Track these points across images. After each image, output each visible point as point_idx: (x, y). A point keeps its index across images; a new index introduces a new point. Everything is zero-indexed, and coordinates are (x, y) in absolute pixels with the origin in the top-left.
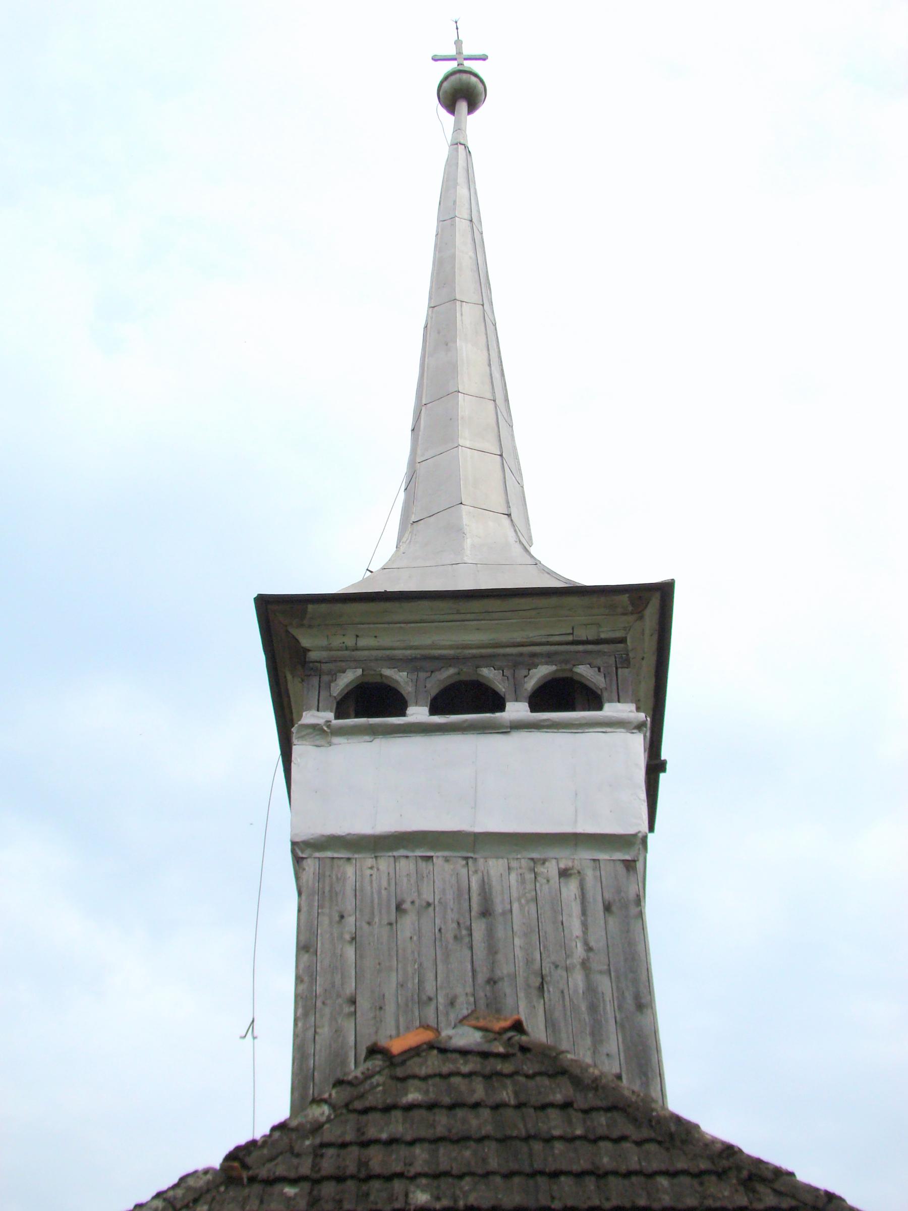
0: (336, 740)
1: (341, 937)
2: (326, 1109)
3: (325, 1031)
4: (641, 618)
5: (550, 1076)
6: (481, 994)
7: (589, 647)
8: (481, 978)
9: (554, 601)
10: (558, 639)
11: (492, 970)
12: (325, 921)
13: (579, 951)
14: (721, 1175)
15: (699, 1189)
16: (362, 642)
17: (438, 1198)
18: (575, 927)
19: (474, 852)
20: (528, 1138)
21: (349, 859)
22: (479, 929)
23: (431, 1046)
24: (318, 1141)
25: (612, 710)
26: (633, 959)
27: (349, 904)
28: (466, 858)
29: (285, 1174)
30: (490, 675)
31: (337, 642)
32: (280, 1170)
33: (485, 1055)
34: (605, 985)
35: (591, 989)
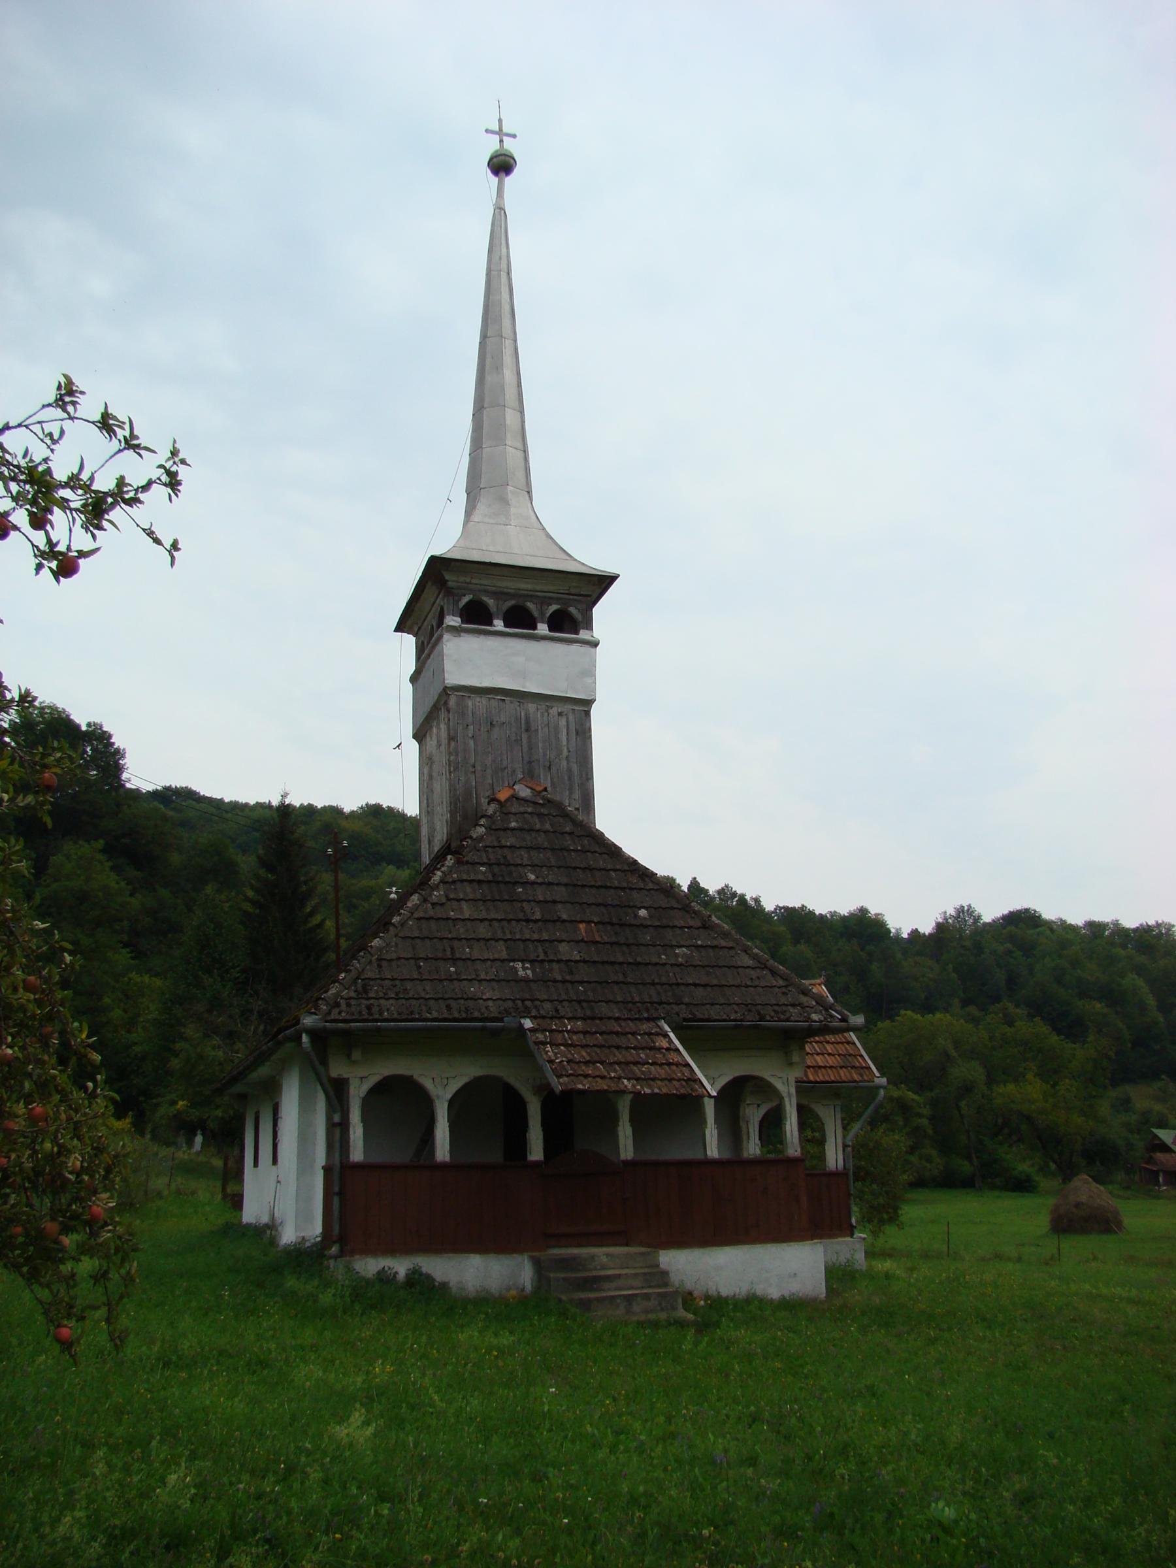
2: (483, 829)
7: (575, 597)
8: (526, 759)
13: (565, 752)
16: (473, 581)
18: (564, 738)
21: (469, 697)
22: (525, 737)
31: (462, 579)
34: (575, 767)
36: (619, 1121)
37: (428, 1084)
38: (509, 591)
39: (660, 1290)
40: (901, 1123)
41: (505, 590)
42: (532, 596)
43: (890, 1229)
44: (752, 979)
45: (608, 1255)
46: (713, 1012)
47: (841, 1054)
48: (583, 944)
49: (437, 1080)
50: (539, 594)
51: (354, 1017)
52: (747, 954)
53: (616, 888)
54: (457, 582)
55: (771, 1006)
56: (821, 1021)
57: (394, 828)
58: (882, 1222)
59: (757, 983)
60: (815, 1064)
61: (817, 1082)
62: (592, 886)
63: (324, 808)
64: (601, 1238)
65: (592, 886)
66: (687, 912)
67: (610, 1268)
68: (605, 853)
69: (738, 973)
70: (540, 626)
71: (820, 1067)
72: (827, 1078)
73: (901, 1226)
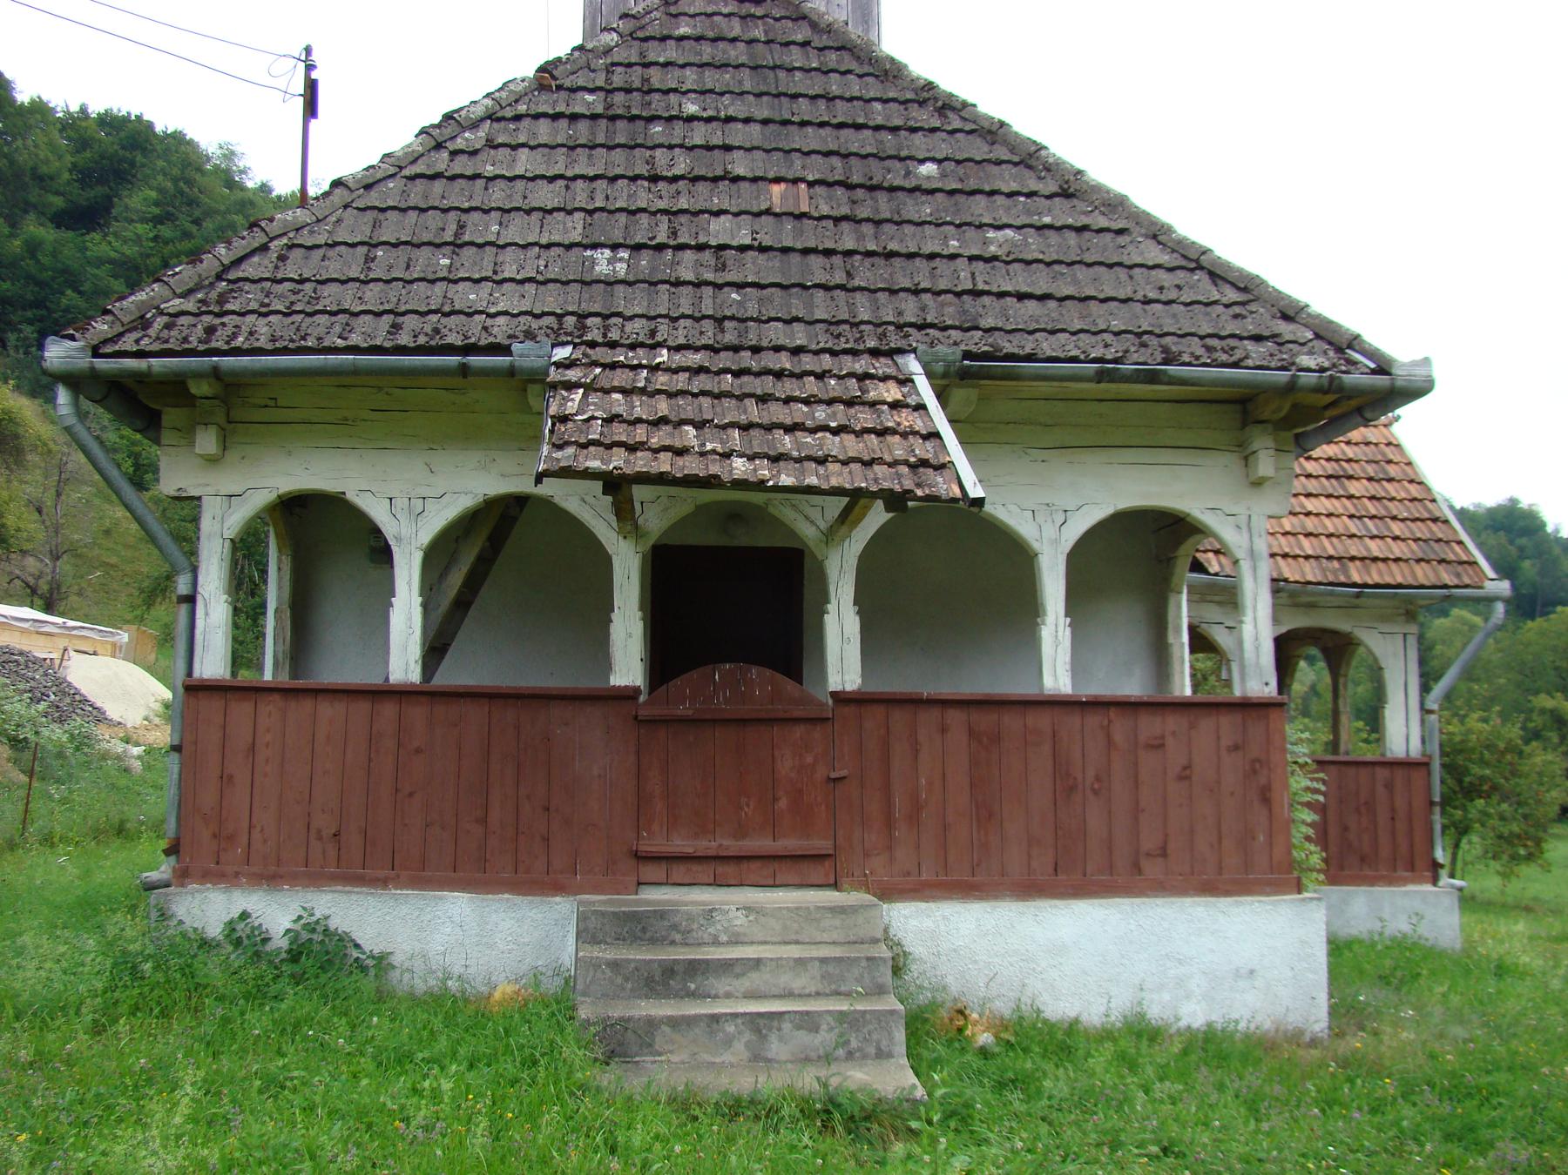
14: (922, 103)
32: (581, 83)
36: (828, 602)
37: (377, 511)
39: (844, 1007)
40: (1556, 740)
43: (1528, 870)
44: (1161, 288)
45: (748, 909)
46: (1048, 346)
47: (1419, 539)
48: (770, 219)
52: (1159, 243)
53: (877, 128)
55: (1202, 338)
56: (1322, 370)
58: (1514, 858)
59: (1173, 295)
60: (1365, 554)
61: (1366, 586)
62: (822, 125)
65: (822, 125)
66: (1030, 167)
69: (1131, 277)
71: (1375, 559)
72: (1389, 580)
73: (1547, 868)
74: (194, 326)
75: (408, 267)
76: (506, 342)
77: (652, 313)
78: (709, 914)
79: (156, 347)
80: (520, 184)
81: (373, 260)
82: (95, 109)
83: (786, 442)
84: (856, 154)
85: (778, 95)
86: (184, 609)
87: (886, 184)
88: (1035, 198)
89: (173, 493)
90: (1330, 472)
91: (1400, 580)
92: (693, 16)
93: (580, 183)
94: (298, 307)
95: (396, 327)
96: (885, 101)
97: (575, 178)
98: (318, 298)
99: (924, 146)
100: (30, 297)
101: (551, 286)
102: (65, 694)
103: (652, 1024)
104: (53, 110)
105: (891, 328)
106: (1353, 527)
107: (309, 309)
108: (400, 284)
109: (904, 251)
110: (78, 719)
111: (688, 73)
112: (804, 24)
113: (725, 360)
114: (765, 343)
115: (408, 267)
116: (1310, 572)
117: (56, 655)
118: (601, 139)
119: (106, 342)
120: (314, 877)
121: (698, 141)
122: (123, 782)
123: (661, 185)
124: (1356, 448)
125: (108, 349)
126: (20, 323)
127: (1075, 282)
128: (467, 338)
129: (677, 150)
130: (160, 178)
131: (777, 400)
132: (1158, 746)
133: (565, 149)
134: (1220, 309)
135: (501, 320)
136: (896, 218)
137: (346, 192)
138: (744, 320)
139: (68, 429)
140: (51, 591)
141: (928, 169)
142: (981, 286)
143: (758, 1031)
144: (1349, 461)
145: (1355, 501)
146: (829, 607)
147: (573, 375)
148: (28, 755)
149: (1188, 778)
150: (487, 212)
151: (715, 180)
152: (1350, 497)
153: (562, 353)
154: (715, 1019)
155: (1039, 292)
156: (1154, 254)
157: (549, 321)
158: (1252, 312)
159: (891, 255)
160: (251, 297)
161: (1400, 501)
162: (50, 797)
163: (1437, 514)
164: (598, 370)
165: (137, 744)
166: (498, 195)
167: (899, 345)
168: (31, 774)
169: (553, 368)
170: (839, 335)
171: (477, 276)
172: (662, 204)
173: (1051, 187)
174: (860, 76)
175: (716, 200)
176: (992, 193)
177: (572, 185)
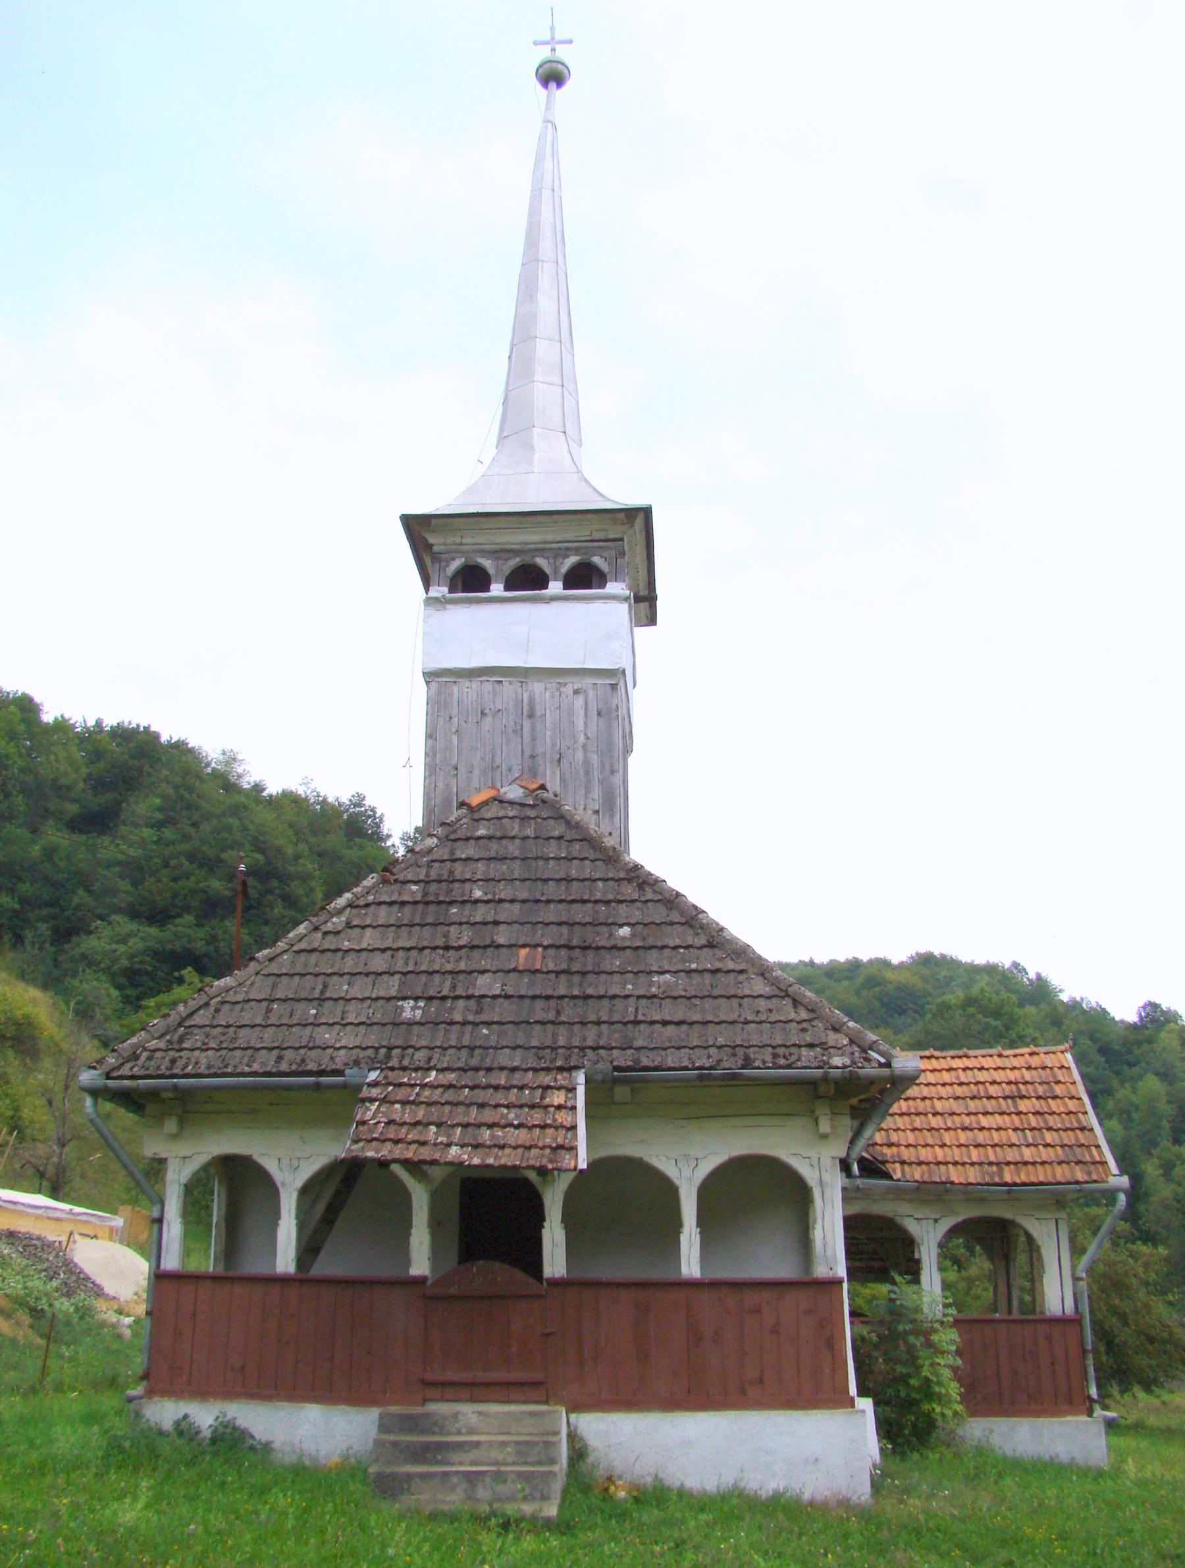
0: (448, 606)
1: (450, 730)
2: (435, 840)
3: (440, 785)
4: (632, 526)
5: (555, 819)
6: (526, 764)
8: (528, 752)
9: (579, 516)
10: (581, 539)
11: (533, 751)
12: (441, 720)
13: (582, 739)
14: (629, 880)
15: (617, 888)
16: (464, 541)
17: (486, 894)
19: (526, 678)
20: (536, 858)
22: (527, 724)
23: (495, 799)
24: (430, 858)
25: (613, 588)
26: (611, 745)
27: (455, 711)
28: (522, 682)
29: (411, 878)
30: (541, 562)
31: (451, 540)
32: (409, 877)
33: (522, 805)
34: (594, 759)
35: (587, 762)
36: (544, 1220)
37: (271, 1166)
38: (513, 546)
41: (508, 547)
42: (544, 550)
44: (758, 1012)
45: (480, 1413)
46: (671, 1059)
49: (285, 1161)
50: (553, 546)
51: (147, 1072)
52: (765, 978)
53: (596, 902)
54: (444, 544)
56: (844, 1067)
57: (945, 976)
59: (763, 1017)
60: (1019, 1159)
61: (1015, 1184)
62: (561, 901)
63: (871, 962)
64: (477, 1390)
66: (692, 927)
67: (483, 1433)
68: (598, 860)
70: (551, 584)
71: (1026, 1163)
72: (1033, 1179)
74: (164, 1058)
75: (291, 1016)
76: (342, 1068)
77: (433, 1045)
78: (456, 1415)
79: (142, 1072)
80: (364, 954)
81: (271, 1011)
82: (110, 722)
83: (486, 1134)
84: (578, 923)
85: (535, 880)
86: (156, 1226)
87: (593, 945)
88: (691, 950)
89: (150, 1156)
90: (1007, 1094)
91: (1041, 1178)
92: (488, 820)
93: (401, 953)
94: (224, 1045)
95: (280, 1058)
96: (607, 880)
97: (398, 949)
98: (236, 1038)
99: (624, 915)
100: (46, 897)
101: (375, 1027)
102: (72, 1273)
103: (409, 1477)
104: (74, 727)
105: (576, 1050)
106: (1014, 1138)
107: (231, 1047)
108: (286, 1028)
109: (595, 994)
110: (82, 1294)
111: (480, 865)
112: (561, 821)
113: (468, 1078)
114: (495, 1066)
115: (291, 1016)
116: (973, 1175)
117: (64, 1238)
118: (417, 920)
119: (113, 1069)
120: (229, 1394)
121: (478, 919)
122: (115, 1346)
123: (451, 952)
124: (1034, 1072)
125: (115, 1074)
126: (37, 921)
127: (703, 1011)
128: (320, 1065)
129: (465, 926)
130: (164, 785)
131: (490, 1105)
132: (756, 1311)
133: (394, 928)
134: (794, 1024)
135: (342, 1052)
136: (596, 970)
137: (257, 964)
138: (488, 1048)
139: (91, 1121)
140: (58, 1174)
141: (625, 931)
142: (640, 1017)
143: (470, 1482)
144: (1025, 1083)
145: (1022, 1116)
146: (545, 1224)
147: (375, 1092)
148: (44, 1323)
149: (778, 1332)
150: (342, 975)
151: (485, 947)
152: (1019, 1113)
153: (373, 1076)
154: (446, 1474)
155: (676, 1020)
156: (759, 987)
157: (370, 1052)
158: (813, 1026)
159: (587, 997)
160: (198, 1038)
161: (1059, 1114)
162: (62, 1357)
163: (1085, 1124)
164: (391, 1088)
165: (128, 1315)
166: (349, 964)
167: (576, 1063)
168: (48, 1338)
169: (365, 1087)
170: (542, 1058)
171: (331, 1021)
172: (449, 967)
173: (702, 940)
174: (592, 861)
175: (483, 963)
176: (663, 947)
177: (396, 954)
